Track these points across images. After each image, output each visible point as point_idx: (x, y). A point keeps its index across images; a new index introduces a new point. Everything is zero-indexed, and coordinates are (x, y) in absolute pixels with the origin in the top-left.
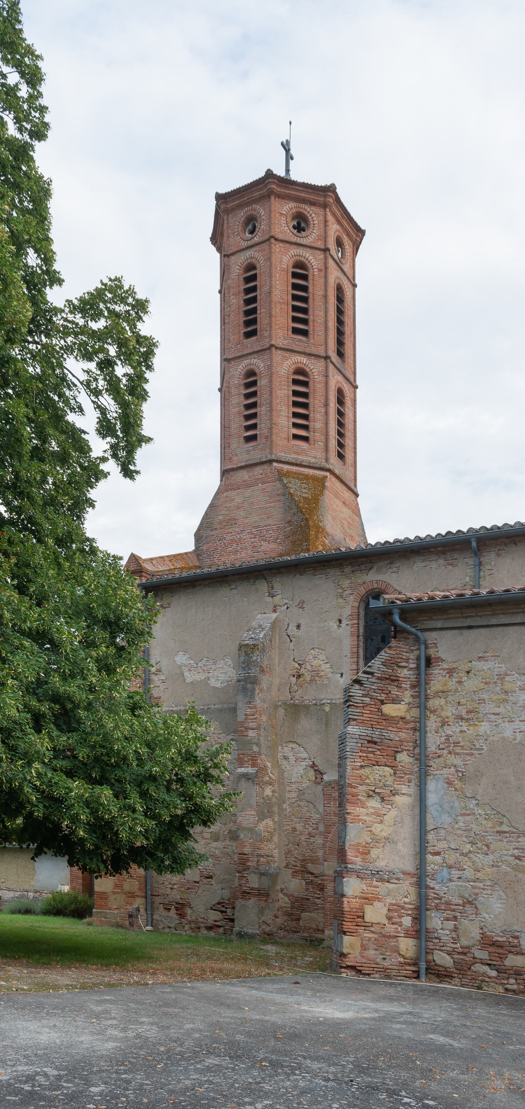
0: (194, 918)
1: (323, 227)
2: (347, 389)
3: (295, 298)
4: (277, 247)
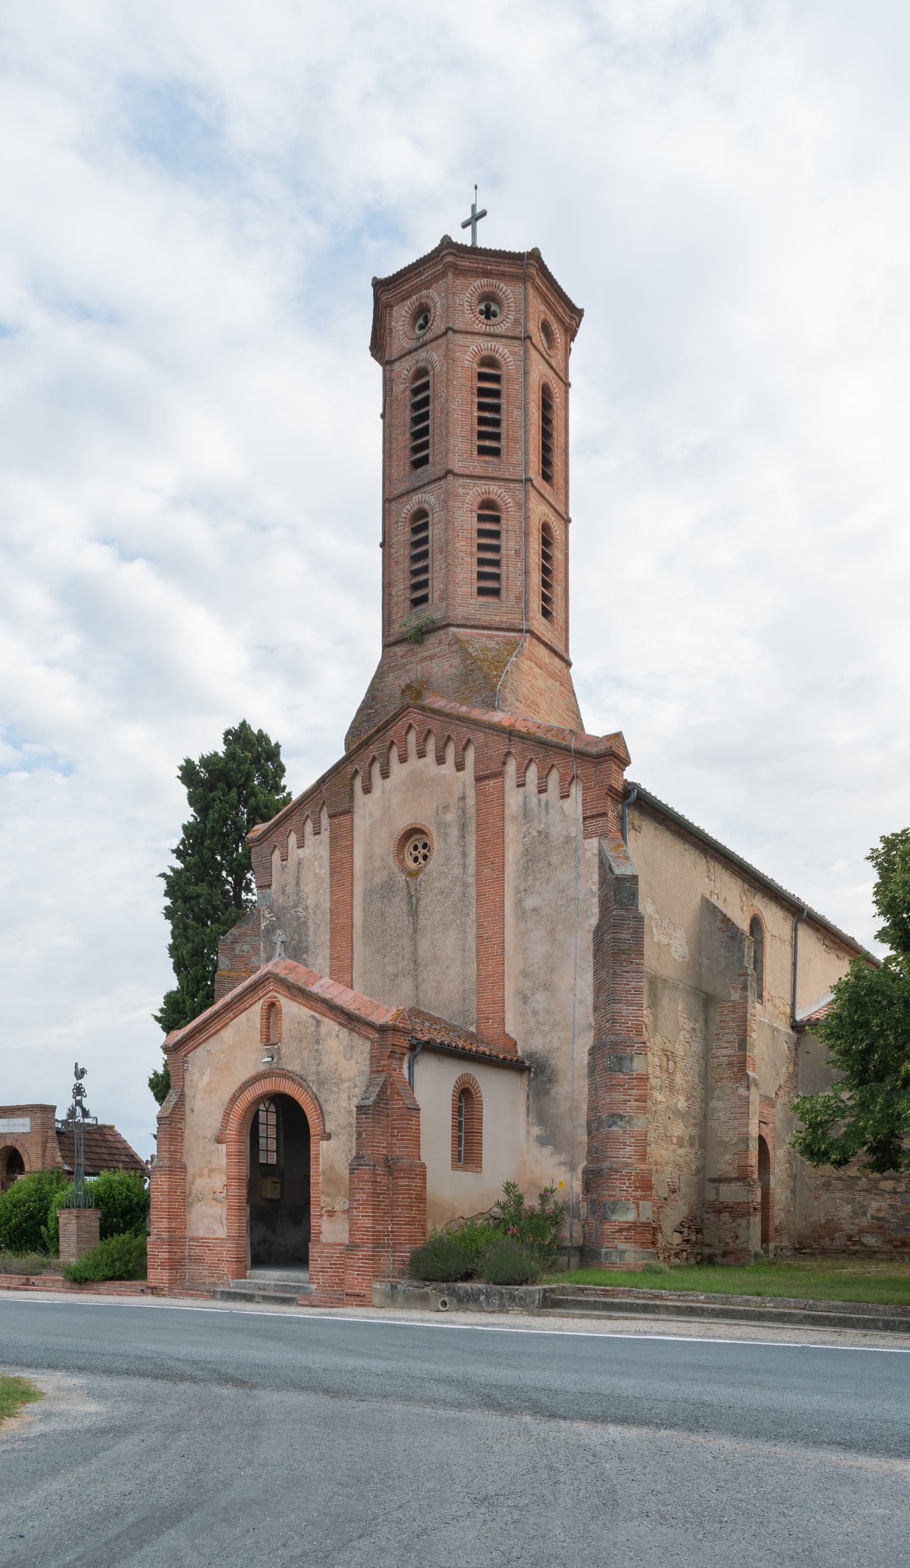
1: (521, 304)
2: (556, 388)
3: (482, 407)
4: (459, 339)
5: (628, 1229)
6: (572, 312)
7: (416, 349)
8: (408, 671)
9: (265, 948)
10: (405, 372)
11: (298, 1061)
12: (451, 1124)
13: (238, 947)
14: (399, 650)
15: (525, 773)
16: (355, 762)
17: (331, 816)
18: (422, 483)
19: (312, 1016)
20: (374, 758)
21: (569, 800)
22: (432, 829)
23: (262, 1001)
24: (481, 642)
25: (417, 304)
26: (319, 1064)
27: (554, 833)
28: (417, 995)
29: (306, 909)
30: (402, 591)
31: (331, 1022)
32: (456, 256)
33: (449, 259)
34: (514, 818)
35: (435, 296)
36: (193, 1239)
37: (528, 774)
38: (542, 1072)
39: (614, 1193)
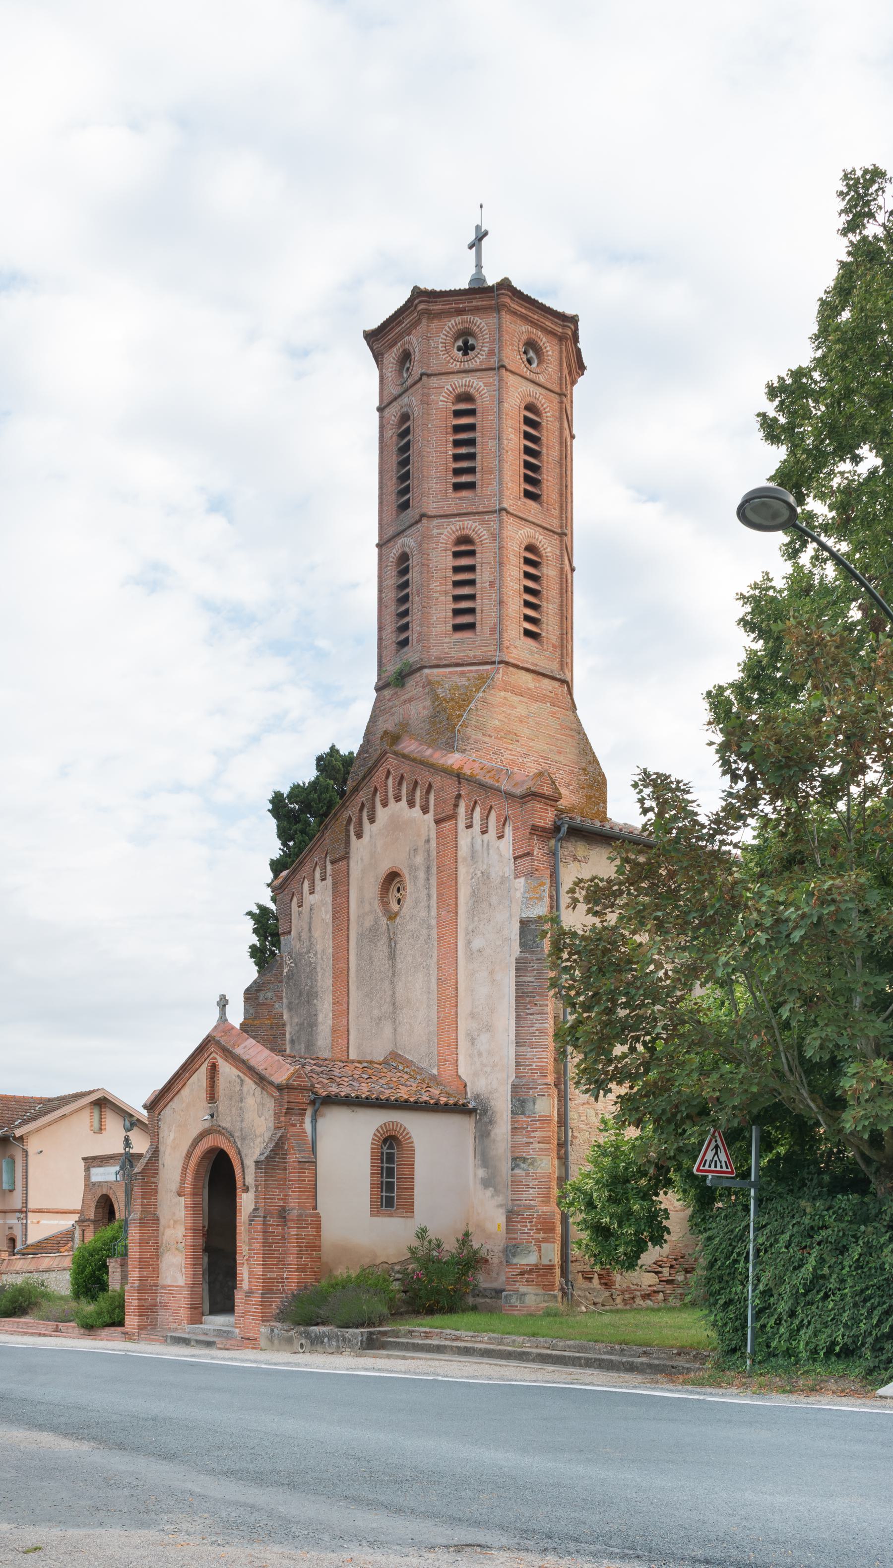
0: (624, 1286)
4: (434, 382)
5: (530, 1272)
6: (563, 321)
7: (400, 395)
8: (393, 715)
9: (287, 994)
10: (393, 418)
11: (229, 1119)
12: (370, 1171)
13: (261, 995)
14: (387, 693)
15: (472, 814)
16: (349, 808)
17: (332, 863)
18: (403, 528)
19: (238, 1076)
20: (363, 805)
21: (504, 840)
22: (405, 872)
23: (207, 1062)
24: (451, 680)
25: (401, 350)
26: (242, 1121)
27: (493, 875)
28: (395, 1039)
29: (315, 955)
30: (391, 637)
31: (250, 1081)
32: (429, 302)
33: (421, 307)
34: (465, 859)
35: (414, 341)
36: (164, 1287)
37: (475, 815)
38: (485, 1113)
39: (515, 1236)
